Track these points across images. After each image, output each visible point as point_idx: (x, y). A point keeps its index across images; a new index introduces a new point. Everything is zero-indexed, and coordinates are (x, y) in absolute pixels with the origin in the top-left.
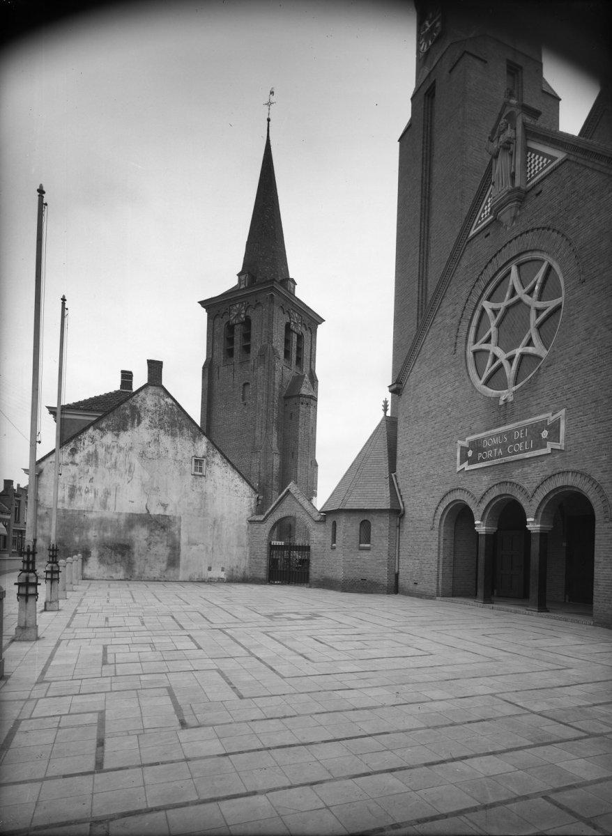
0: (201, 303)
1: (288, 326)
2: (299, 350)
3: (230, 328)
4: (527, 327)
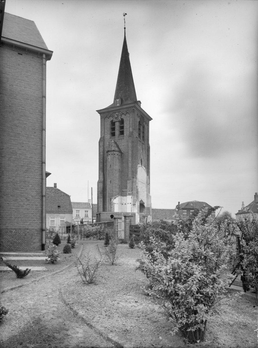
0: (51, 174)
3: (113, 123)
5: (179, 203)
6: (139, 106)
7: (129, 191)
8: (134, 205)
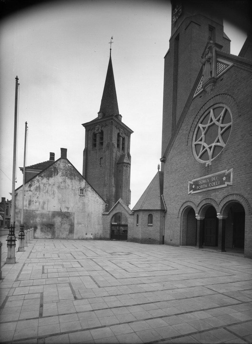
0: (83, 125)
1: (118, 134)
2: (123, 144)
3: (95, 135)
4: (217, 135)
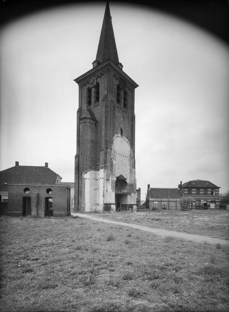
0: (74, 80)
2: (125, 100)
3: (89, 90)
5: (181, 182)
6: (118, 67)
7: (102, 164)
8: (108, 180)
